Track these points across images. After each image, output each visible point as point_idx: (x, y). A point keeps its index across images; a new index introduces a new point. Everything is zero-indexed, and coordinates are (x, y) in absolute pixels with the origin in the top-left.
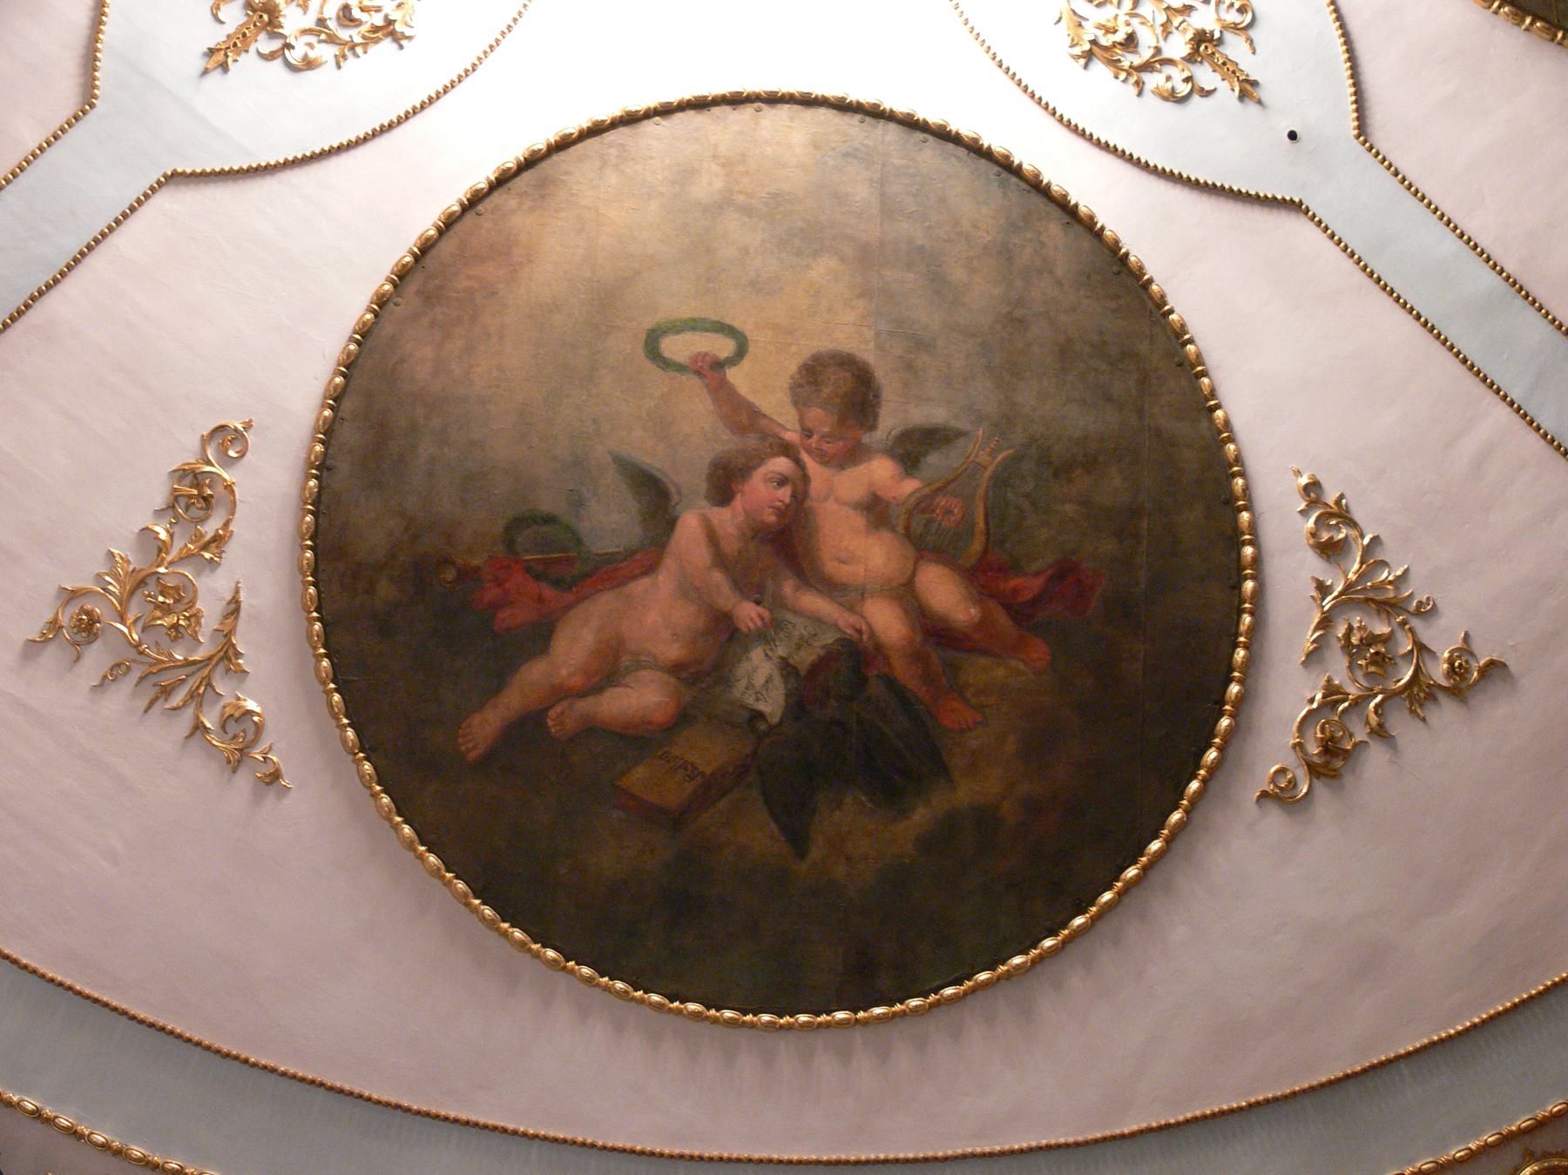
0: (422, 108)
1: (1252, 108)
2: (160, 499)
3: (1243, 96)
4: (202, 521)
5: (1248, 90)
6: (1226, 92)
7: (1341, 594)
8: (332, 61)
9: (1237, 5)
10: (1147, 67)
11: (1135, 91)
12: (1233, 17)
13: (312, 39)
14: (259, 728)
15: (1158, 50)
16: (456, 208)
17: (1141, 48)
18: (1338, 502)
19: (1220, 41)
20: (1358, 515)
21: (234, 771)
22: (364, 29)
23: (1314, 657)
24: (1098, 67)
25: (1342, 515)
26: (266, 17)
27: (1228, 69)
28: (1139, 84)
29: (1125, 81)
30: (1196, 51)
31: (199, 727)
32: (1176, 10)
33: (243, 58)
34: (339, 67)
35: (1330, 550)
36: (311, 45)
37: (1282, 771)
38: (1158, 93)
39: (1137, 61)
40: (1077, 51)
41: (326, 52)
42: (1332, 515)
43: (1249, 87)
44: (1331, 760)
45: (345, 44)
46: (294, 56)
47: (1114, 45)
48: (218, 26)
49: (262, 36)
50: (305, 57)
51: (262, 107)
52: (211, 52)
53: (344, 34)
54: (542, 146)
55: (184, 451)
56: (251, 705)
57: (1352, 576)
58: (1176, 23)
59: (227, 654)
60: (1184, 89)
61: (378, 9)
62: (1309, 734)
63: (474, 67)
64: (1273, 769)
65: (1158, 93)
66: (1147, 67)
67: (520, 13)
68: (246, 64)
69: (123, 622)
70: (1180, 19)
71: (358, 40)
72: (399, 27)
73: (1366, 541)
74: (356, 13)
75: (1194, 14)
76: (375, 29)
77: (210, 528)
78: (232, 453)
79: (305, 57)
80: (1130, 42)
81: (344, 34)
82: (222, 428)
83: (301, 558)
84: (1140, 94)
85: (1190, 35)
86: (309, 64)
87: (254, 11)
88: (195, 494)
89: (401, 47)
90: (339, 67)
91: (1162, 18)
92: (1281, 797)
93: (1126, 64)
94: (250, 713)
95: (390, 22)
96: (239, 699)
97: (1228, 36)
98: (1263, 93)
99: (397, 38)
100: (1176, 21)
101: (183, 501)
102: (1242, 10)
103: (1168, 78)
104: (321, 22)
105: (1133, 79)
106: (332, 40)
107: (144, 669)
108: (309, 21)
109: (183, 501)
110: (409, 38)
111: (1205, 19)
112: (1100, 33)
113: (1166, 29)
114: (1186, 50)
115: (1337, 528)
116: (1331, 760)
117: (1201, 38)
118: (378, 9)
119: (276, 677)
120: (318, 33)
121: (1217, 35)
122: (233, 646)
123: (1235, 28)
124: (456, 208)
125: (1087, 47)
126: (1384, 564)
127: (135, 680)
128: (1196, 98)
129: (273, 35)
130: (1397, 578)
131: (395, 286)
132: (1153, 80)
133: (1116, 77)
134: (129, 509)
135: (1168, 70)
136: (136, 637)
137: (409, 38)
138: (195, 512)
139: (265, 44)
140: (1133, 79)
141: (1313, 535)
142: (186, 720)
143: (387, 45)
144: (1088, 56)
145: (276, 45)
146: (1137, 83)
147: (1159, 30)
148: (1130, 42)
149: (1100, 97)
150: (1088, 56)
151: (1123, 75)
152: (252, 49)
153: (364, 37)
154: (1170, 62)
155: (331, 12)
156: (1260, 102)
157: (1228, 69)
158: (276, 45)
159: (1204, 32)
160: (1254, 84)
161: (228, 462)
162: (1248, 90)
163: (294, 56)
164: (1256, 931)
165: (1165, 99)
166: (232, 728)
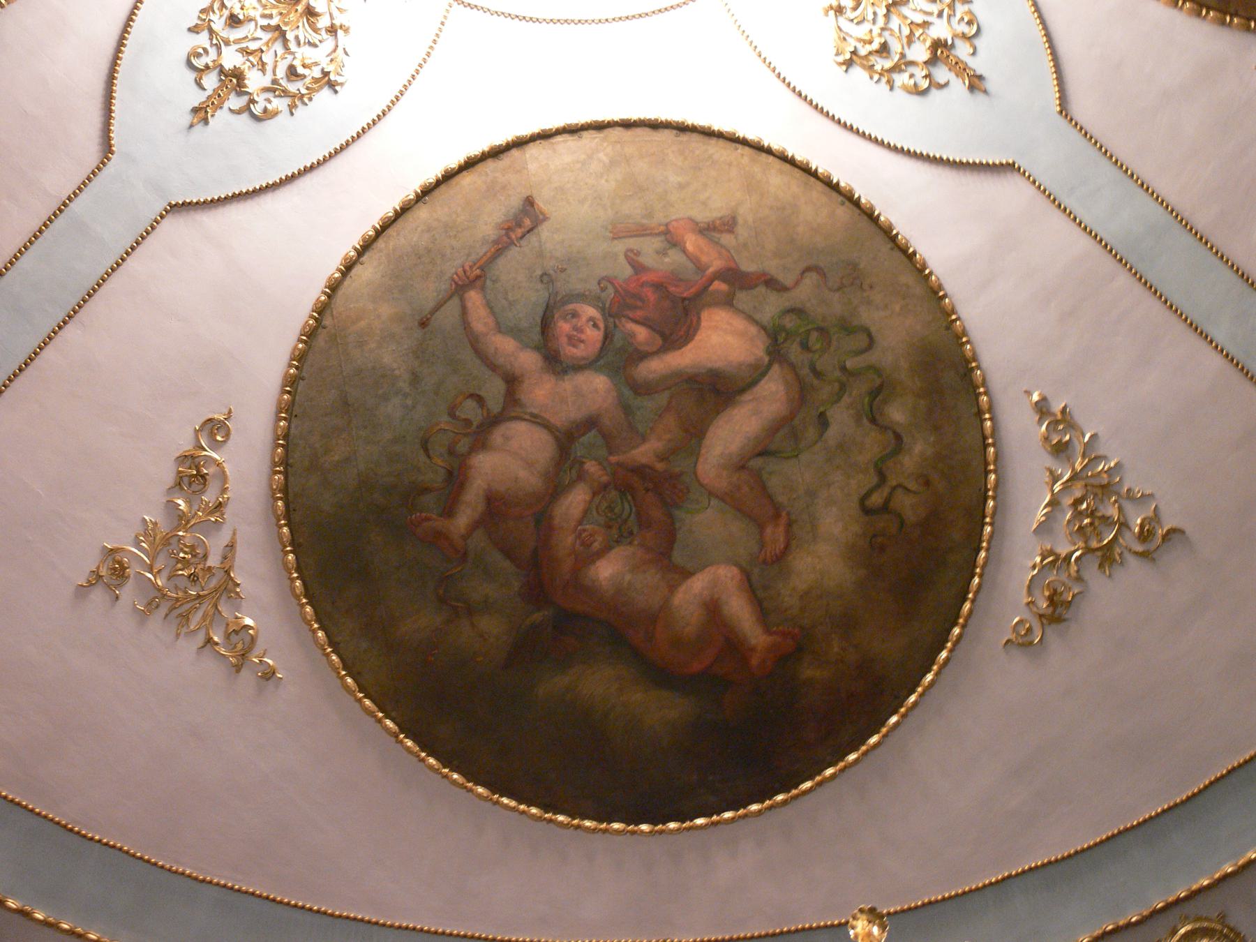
0: (359, 136)
1: (980, 97)
2: (169, 477)
3: (972, 88)
4: (202, 492)
5: (976, 83)
6: (958, 86)
7: (1067, 481)
8: (285, 109)
9: (966, 19)
10: (896, 69)
11: (888, 87)
12: (963, 28)
13: (270, 95)
14: (253, 640)
15: (903, 55)
16: (371, 233)
17: (893, 54)
18: (1064, 410)
19: (953, 45)
20: (1079, 417)
21: (238, 671)
22: (308, 80)
23: (1044, 528)
24: (858, 72)
25: (1065, 420)
26: (234, 81)
27: (960, 68)
28: (194, 30)
29: (878, 81)
30: (934, 52)
31: (209, 640)
32: (918, 25)
33: (218, 113)
34: (292, 114)
35: (1060, 450)
36: (269, 101)
37: (1021, 622)
38: (905, 88)
39: (888, 64)
40: (841, 59)
41: (280, 104)
42: (1057, 422)
43: (976, 80)
44: (1057, 611)
45: (294, 96)
46: (257, 109)
47: (870, 53)
48: (201, 91)
49: (232, 96)
50: (265, 110)
51: (239, 148)
52: (195, 110)
53: (292, 88)
54: (432, 180)
55: (185, 444)
56: (248, 621)
57: (1078, 467)
58: (917, 34)
59: (228, 587)
60: (924, 84)
61: (316, 64)
62: (1037, 592)
63: (428, 54)
64: (1016, 620)
65: (905, 88)
66: (896, 69)
67: (437, 35)
68: (221, 119)
69: (151, 572)
70: (921, 31)
71: (304, 91)
72: (332, 77)
73: (1086, 439)
74: (300, 70)
75: (932, 28)
76: (316, 80)
77: (209, 497)
78: (219, 438)
79: (265, 110)
80: (884, 49)
81: (292, 88)
82: (210, 420)
83: (274, 508)
84: (892, 88)
85: (928, 43)
86: (268, 115)
87: (226, 76)
88: (193, 474)
89: (336, 92)
90: (292, 114)
91: (906, 31)
92: (1022, 643)
93: (878, 68)
94: (247, 627)
95: (326, 74)
96: (237, 618)
97: (958, 42)
98: (989, 85)
99: (332, 85)
100: (918, 33)
101: (186, 480)
102: (970, 23)
103: (912, 76)
104: (275, 82)
105: (884, 80)
106: (285, 93)
107: (169, 604)
108: (266, 81)
109: (186, 480)
110: (342, 84)
111: (940, 30)
112: (859, 46)
113: (910, 39)
114: (926, 56)
115: (1064, 432)
116: (1057, 611)
117: (937, 45)
118: (316, 64)
119: (263, 596)
120: (274, 91)
121: (950, 42)
122: (232, 579)
123: (963, 36)
124: (371, 233)
125: (848, 56)
126: (1104, 458)
127: (163, 615)
128: (934, 91)
129: (240, 94)
130: (1110, 469)
131: (329, 296)
132: (901, 79)
133: (871, 78)
134: (144, 499)
135: (912, 69)
136: (160, 583)
137: (342, 84)
138: (195, 487)
139: (235, 102)
140: (884, 80)
141: (1046, 439)
142: (201, 638)
143: (326, 92)
144: (849, 64)
145: (243, 101)
146: (888, 82)
147: (905, 40)
148: (884, 49)
149: (860, 97)
150: (849, 64)
151: (876, 77)
152: (226, 105)
153: (308, 88)
154: (912, 63)
155: (281, 73)
156: (985, 92)
157: (960, 68)
158: (243, 101)
159: (939, 40)
160: (980, 77)
161: (216, 445)
162: (976, 83)
163: (257, 109)
164: (984, 762)
165: (910, 92)
166: (234, 638)
